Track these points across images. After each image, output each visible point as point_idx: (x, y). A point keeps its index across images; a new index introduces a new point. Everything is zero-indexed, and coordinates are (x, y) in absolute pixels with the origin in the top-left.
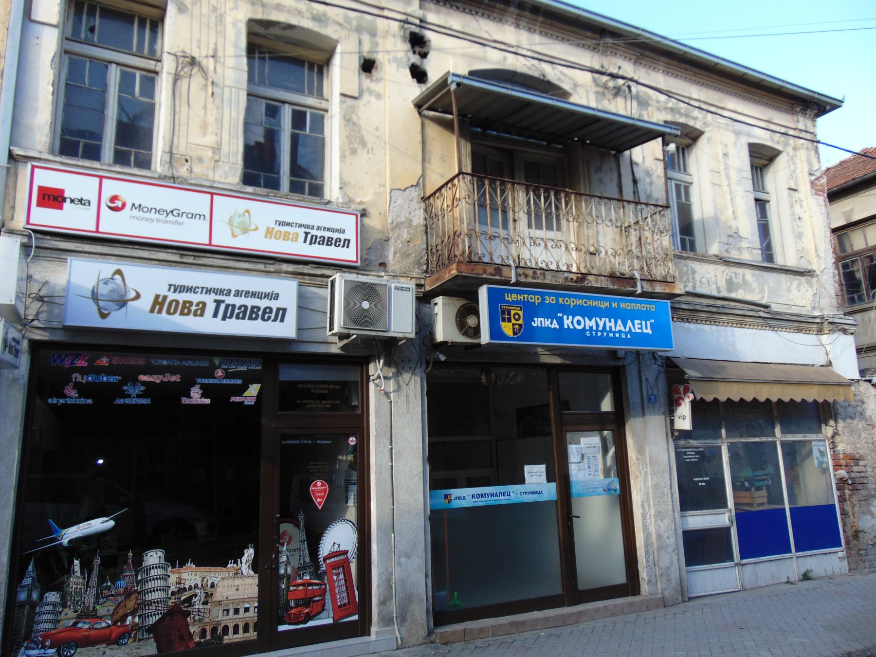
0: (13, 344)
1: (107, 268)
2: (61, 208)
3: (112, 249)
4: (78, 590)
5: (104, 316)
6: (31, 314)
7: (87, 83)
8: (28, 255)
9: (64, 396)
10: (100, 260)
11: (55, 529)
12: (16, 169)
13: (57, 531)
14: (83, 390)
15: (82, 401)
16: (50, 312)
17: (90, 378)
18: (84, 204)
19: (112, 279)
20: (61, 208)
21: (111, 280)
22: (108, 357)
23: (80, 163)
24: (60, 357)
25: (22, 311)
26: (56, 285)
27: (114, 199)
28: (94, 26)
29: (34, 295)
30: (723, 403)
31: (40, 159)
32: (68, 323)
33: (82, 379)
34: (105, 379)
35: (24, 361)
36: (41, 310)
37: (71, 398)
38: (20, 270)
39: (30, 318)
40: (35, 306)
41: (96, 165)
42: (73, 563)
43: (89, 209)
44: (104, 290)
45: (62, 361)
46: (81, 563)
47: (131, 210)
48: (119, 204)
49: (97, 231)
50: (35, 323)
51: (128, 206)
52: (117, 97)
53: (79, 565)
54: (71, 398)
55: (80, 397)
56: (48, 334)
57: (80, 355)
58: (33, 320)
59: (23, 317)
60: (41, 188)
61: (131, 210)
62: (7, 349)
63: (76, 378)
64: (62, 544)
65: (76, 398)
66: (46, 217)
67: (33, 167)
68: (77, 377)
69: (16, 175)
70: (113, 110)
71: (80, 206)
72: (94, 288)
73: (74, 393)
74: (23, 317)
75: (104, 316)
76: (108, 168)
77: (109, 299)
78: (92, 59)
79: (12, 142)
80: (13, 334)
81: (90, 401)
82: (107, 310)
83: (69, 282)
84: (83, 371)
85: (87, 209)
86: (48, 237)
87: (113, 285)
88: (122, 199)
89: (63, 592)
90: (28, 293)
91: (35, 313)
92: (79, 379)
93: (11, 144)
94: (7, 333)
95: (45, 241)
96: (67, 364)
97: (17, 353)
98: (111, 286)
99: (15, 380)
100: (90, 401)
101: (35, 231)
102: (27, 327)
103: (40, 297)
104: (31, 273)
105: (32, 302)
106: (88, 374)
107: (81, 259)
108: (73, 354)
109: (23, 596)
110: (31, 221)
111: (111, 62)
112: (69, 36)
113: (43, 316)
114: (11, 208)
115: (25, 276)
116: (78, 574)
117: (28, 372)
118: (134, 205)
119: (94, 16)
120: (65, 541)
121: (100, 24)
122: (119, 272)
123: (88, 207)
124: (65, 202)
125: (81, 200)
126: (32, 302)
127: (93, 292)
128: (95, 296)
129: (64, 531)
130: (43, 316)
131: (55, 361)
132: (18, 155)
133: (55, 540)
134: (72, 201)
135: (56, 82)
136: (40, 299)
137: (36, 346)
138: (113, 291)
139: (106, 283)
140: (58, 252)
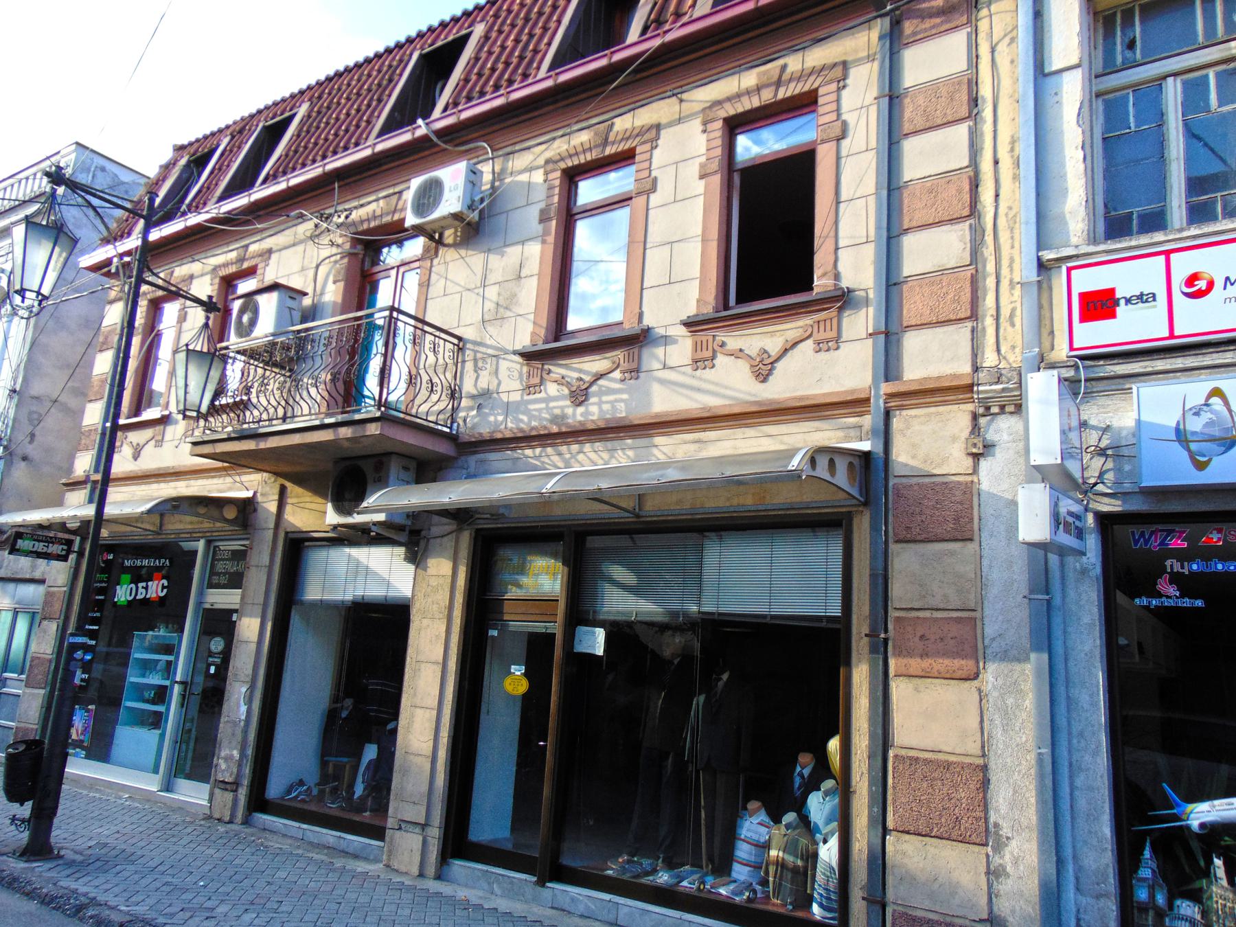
0: (1070, 519)
1: (1196, 390)
2: (1112, 315)
3: (1200, 358)
4: (1227, 910)
5: (1200, 466)
6: (1092, 476)
7: (1132, 125)
8: (1076, 394)
9: (1159, 595)
10: (1183, 379)
11: (1175, 801)
12: (1050, 280)
13: (1178, 805)
14: (1187, 584)
15: (1186, 602)
16: (1118, 470)
17: (1195, 567)
18: (1147, 301)
19: (1207, 405)
20: (1112, 315)
21: (1205, 408)
22: (1220, 531)
23: (1133, 243)
24: (1142, 534)
25: (1077, 475)
26: (1121, 429)
27: (1192, 279)
28: (1135, 37)
29: (1093, 448)
30: (63, 496)
31: (1077, 256)
32: (1147, 483)
33: (1182, 567)
34: (1220, 567)
35: (1092, 543)
36: (1104, 469)
37: (1168, 597)
38: (1064, 413)
39: (1092, 481)
40: (1098, 462)
41: (1159, 237)
42: (1212, 862)
43: (1155, 306)
44: (1195, 425)
45: (1146, 542)
46: (1225, 864)
47: (1225, 288)
48: (1202, 285)
49: (1172, 336)
50: (1100, 488)
51: (1219, 284)
52: (1181, 123)
53: (1223, 868)
54: (1168, 597)
55: (1182, 596)
56: (1119, 503)
57: (1173, 531)
58: (1095, 484)
59: (1080, 481)
60: (1083, 296)
61: (1225, 288)
62: (1061, 526)
63: (1172, 566)
64: (1188, 827)
65: (1177, 597)
66: (1094, 334)
67: (1069, 270)
68: (1172, 565)
69: (1050, 289)
70: (1178, 145)
71: (1140, 305)
72: (1178, 423)
73: (1172, 591)
74: (1080, 481)
75: (1200, 466)
76: (1178, 236)
77: (1206, 437)
78: (1135, 87)
79: (1040, 246)
80: (1068, 505)
81: (1199, 603)
82: (1204, 456)
83: (1138, 422)
84: (1183, 556)
85: (1151, 307)
86: (1102, 363)
87: (1209, 415)
88: (1206, 276)
89: (1203, 905)
90: (1084, 447)
91: (1097, 474)
92: (1177, 567)
93: (1039, 248)
94: (1056, 505)
95: (1096, 369)
96: (1154, 544)
97: (1080, 533)
98: (1206, 416)
99: (1084, 572)
100: (1199, 603)
101: (1082, 358)
102: (1089, 494)
103: (1101, 449)
104: (1084, 417)
105: (1091, 459)
106: (1191, 560)
107: (1153, 383)
108: (1163, 531)
109: (1142, 894)
110: (1076, 346)
111: (1165, 78)
112: (1100, 70)
113: (1110, 476)
114: (1049, 334)
115: (1075, 423)
116: (1224, 883)
117: (1100, 559)
118: (1227, 279)
119: (1133, 25)
120: (1195, 824)
121: (1143, 31)
122: (1216, 392)
123: (1153, 303)
124: (1118, 305)
125: (1140, 297)
126: (1091, 459)
127: (1177, 430)
128: (1181, 436)
129: (1190, 807)
130: (1110, 476)
131: (1136, 542)
132: (1048, 260)
133: (1176, 818)
134: (1128, 301)
135: (1088, 141)
136: (1102, 452)
137: (1105, 520)
138: (1210, 424)
139: (1197, 414)
140: (1118, 380)
